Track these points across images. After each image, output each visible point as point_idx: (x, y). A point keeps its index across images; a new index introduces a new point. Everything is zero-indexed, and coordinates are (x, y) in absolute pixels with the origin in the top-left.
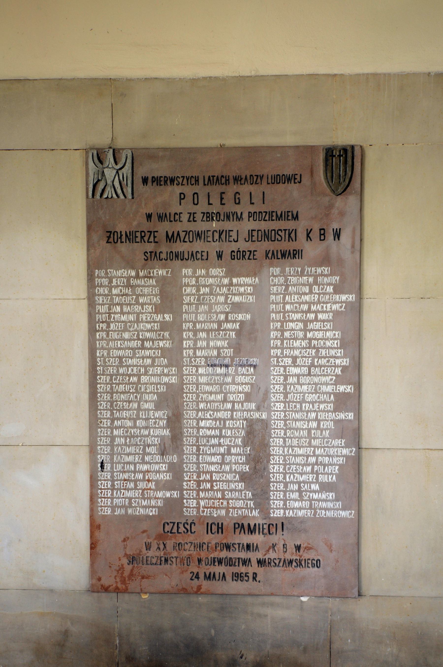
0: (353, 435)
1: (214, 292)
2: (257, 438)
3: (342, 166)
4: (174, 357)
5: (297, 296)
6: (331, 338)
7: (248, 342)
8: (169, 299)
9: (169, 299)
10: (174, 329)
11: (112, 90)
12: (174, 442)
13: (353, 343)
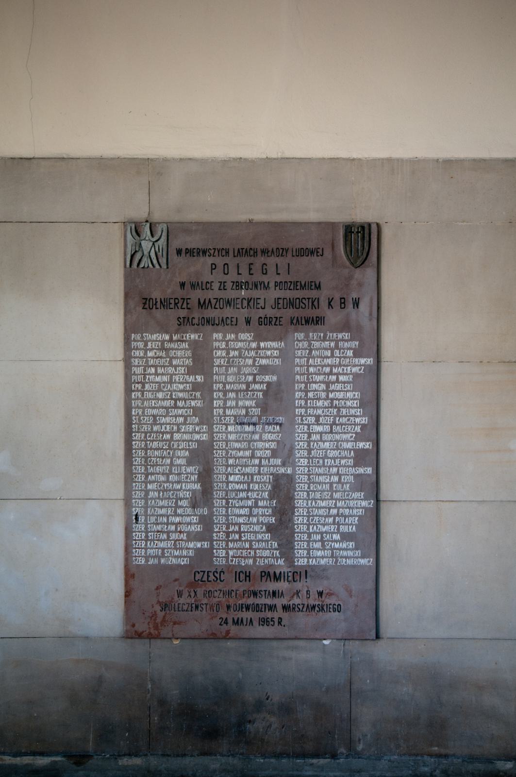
0: (373, 488)
1: (242, 354)
2: (282, 491)
3: (361, 242)
4: (205, 416)
5: (323, 360)
6: (351, 398)
7: (275, 401)
8: (201, 361)
9: (201, 361)
10: (205, 389)
11: (150, 169)
12: (204, 497)
13: (373, 403)
